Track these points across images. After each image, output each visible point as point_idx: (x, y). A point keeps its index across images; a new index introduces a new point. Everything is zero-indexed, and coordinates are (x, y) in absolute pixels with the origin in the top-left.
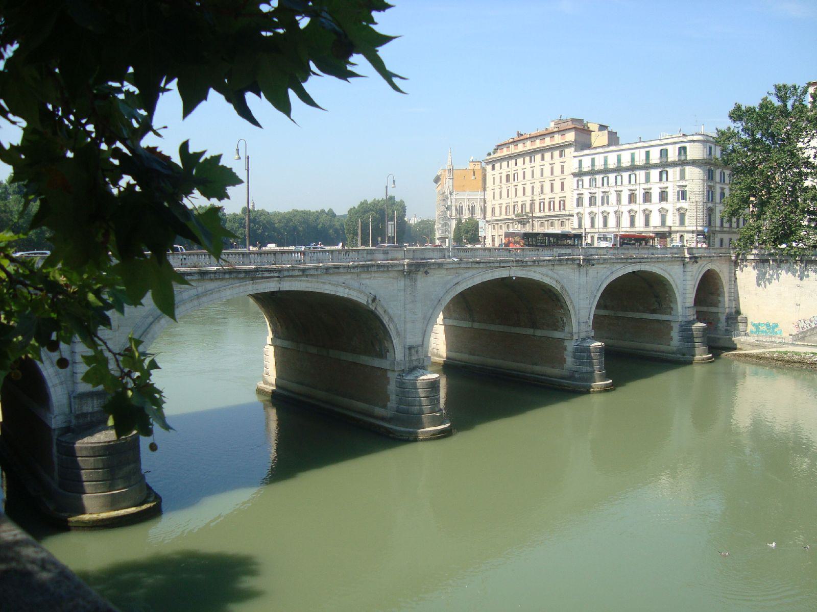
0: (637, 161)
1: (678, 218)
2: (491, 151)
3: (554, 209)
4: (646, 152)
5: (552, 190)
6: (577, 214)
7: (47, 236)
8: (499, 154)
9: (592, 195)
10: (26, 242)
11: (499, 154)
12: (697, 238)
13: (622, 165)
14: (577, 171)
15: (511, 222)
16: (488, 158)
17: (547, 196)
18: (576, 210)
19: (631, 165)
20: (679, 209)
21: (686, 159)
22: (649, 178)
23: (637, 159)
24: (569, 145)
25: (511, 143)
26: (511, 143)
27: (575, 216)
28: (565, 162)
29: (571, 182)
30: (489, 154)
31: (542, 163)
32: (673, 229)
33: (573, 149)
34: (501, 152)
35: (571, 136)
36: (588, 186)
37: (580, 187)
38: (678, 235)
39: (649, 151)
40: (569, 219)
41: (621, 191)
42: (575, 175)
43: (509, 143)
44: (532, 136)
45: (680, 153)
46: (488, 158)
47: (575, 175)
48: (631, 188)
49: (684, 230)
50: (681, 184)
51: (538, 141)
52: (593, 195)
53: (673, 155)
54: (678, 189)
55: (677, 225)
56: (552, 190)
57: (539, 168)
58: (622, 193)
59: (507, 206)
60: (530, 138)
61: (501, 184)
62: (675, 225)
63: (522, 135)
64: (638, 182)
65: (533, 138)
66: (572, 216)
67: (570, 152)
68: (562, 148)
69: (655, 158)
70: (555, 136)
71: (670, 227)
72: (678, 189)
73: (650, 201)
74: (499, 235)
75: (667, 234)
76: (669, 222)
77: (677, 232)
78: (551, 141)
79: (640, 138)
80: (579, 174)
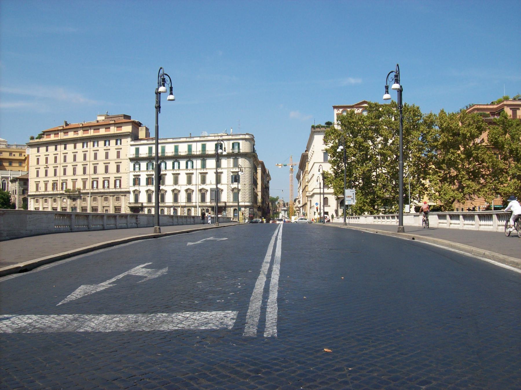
0: (194, 152)
1: (200, 196)
2: (36, 136)
3: (97, 187)
4: (117, 152)
5: (46, 175)
6: (134, 191)
7: (345, 115)
8: (45, 139)
9: (149, 176)
10: (471, 145)
11: (45, 139)
12: (250, 211)
13: (179, 154)
14: (134, 156)
15: (59, 196)
16: (31, 141)
17: (60, 178)
18: (132, 189)
19: (188, 154)
20: (233, 190)
21: (239, 152)
22: (205, 165)
23: (207, 148)
24: (125, 135)
25: (61, 130)
26: (61, 130)
27: (132, 193)
28: (121, 149)
29: (127, 166)
30: (32, 138)
31: (56, 152)
32: (228, 204)
33: (129, 139)
34: (46, 138)
35: (128, 129)
36: (185, 168)
37: (137, 169)
38: (232, 209)
39: (120, 151)
40: (125, 196)
41: (179, 174)
42: (131, 160)
43: (58, 130)
44: (84, 126)
45: (233, 147)
46: (31, 141)
47: (131, 160)
48: (136, 174)
49: (152, 205)
50: (202, 171)
51: (92, 131)
52: (151, 176)
53: (228, 147)
54: (232, 174)
55: (231, 201)
56: (46, 175)
57: (63, 156)
58: (166, 176)
59: (54, 183)
60: (82, 127)
61: (47, 165)
62: (229, 201)
63: (68, 125)
64: (195, 167)
65: (75, 129)
66: (129, 192)
67: (127, 142)
68: (118, 137)
69: (211, 149)
70: (111, 127)
71: (225, 203)
72: (232, 174)
73: (139, 184)
74: (104, 207)
75: (140, 209)
76: (140, 200)
77: (146, 207)
78: (55, 137)
79: (191, 134)
80: (136, 160)
